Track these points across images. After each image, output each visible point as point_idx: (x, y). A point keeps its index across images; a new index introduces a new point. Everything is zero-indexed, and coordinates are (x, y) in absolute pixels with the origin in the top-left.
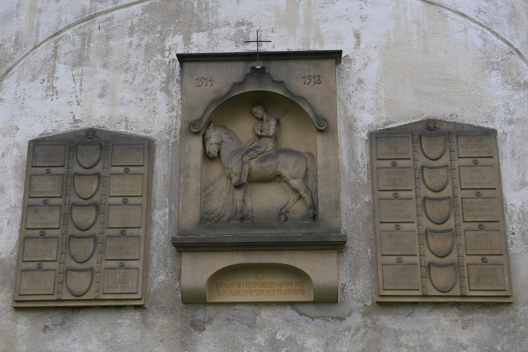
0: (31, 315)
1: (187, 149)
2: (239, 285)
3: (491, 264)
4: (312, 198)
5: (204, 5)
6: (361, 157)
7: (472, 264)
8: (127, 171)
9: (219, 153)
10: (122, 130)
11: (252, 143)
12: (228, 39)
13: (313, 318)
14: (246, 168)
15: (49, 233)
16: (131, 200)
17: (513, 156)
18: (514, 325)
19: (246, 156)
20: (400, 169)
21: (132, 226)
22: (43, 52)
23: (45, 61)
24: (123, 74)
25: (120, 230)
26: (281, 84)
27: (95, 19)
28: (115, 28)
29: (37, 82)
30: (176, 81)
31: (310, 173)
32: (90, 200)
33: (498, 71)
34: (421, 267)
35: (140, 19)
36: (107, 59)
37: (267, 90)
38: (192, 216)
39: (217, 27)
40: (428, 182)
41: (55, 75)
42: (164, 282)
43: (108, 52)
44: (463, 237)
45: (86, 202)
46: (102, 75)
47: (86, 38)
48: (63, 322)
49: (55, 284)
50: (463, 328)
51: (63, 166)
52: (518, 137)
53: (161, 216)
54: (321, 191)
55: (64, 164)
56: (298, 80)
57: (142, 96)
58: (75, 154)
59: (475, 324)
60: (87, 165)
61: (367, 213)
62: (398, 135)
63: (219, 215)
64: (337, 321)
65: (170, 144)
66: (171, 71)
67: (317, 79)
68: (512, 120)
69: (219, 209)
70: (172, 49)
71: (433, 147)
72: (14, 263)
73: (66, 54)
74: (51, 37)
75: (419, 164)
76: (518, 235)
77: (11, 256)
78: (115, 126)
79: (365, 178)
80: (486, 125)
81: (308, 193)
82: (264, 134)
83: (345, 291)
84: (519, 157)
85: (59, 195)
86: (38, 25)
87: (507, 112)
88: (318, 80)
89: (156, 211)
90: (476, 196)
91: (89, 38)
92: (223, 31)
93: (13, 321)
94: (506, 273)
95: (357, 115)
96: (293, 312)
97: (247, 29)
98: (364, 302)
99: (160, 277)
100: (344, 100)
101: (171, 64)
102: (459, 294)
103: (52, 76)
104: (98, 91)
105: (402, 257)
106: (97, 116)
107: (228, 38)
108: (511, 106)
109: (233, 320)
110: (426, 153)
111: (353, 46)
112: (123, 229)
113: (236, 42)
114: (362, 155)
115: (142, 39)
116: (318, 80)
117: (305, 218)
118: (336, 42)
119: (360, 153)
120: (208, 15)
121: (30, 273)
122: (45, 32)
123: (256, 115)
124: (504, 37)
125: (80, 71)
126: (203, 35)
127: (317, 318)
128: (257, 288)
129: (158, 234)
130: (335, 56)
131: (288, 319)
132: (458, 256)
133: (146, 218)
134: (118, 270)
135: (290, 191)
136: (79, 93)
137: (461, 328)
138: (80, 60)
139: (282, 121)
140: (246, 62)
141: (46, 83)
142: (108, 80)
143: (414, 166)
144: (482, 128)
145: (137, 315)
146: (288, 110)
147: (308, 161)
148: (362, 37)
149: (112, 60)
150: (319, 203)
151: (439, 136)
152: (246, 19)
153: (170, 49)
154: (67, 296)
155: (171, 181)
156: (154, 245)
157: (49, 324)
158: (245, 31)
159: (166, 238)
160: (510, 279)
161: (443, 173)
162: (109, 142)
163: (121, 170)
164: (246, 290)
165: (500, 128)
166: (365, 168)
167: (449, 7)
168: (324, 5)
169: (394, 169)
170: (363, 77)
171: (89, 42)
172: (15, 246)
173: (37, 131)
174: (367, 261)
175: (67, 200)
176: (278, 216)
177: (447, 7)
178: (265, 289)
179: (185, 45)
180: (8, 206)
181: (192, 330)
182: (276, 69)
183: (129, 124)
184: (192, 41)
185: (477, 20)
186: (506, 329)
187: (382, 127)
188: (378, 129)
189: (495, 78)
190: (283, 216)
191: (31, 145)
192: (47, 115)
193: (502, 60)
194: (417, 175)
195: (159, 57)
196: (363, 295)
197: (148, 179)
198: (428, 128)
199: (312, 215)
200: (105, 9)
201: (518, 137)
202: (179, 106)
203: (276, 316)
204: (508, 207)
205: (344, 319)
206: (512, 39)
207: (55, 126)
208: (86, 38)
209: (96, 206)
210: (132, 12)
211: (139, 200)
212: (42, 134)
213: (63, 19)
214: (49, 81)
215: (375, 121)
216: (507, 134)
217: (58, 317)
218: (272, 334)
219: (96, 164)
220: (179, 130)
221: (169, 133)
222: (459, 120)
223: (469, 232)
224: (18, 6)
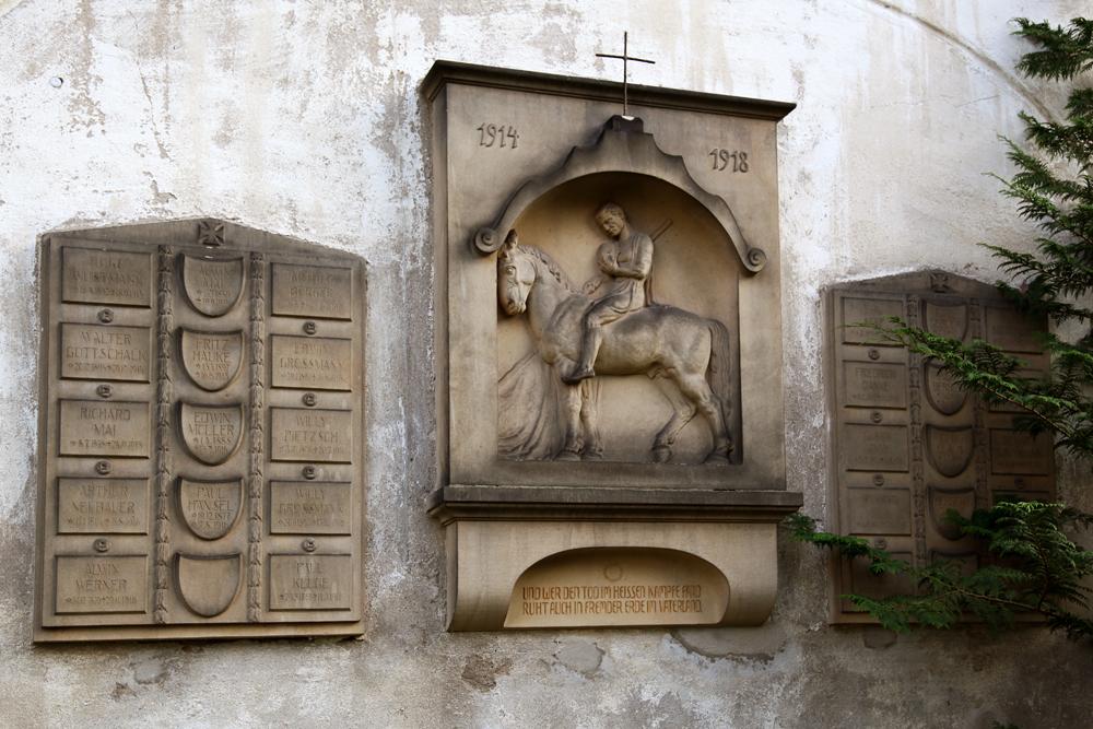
0: (79, 659)
1: (464, 289)
2: (569, 592)
4: (723, 415)
6: (807, 336)
8: (308, 329)
10: (284, 230)
12: (529, 43)
13: (712, 657)
15: (117, 467)
16: (322, 399)
21: (331, 459)
30: (409, 127)
36: (230, 48)
37: (647, 172)
41: (91, 70)
42: (402, 584)
45: (212, 398)
48: (164, 676)
50: (976, 670)
56: (699, 156)
57: (329, 152)
60: (209, 309)
64: (758, 663)
65: (402, 275)
66: (396, 101)
69: (528, 430)
70: (396, 46)
75: (172, 322)
77: (15, 521)
78: (263, 218)
88: (741, 163)
89: (375, 427)
93: (33, 674)
96: (674, 645)
101: (396, 82)
103: (84, 73)
104: (212, 125)
105: (886, 538)
107: (528, 38)
109: (554, 664)
112: (308, 467)
116: (741, 163)
123: (607, 227)
125: (161, 68)
127: (721, 656)
128: (607, 598)
129: (384, 477)
135: (675, 395)
136: (163, 125)
140: (590, 102)
141: (67, 88)
143: (910, 361)
145: (344, 656)
146: (672, 223)
147: (716, 336)
149: (244, 53)
155: (409, 361)
156: (375, 503)
157: (128, 679)
158: (565, 30)
159: (403, 489)
163: (296, 326)
164: (583, 602)
167: (969, 44)
169: (873, 366)
170: (809, 167)
173: (59, 214)
176: (653, 449)
177: (964, 42)
178: (623, 601)
179: (426, 42)
181: (467, 686)
182: (661, 125)
186: (1043, 670)
190: (659, 446)
194: (915, 379)
195: (364, 62)
196: (805, 612)
198: (934, 288)
199: (726, 449)
202: (420, 186)
207: (105, 203)
211: (342, 401)
214: (75, 84)
215: (832, 264)
217: (148, 665)
218: (632, 691)
220: (421, 244)
221: (398, 249)
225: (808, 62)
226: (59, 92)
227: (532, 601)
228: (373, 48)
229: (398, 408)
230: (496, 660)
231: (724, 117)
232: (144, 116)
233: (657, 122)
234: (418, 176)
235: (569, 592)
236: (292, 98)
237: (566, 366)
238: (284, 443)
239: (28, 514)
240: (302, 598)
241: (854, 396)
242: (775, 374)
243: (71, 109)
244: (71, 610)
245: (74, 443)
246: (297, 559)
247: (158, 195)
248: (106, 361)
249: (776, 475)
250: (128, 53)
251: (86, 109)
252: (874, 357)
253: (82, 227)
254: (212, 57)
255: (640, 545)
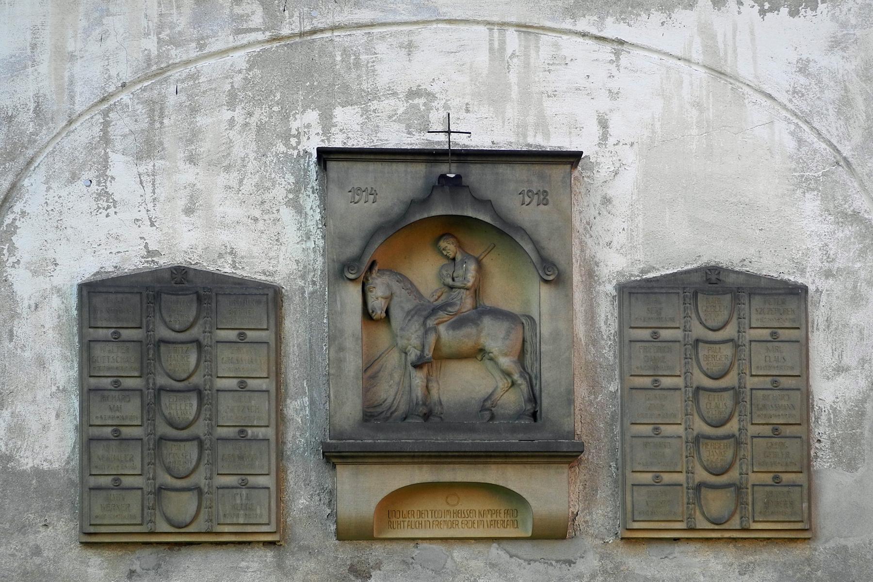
0: (107, 553)
2: (421, 513)
3: (785, 486)
5: (353, 57)
6: (606, 323)
7: (760, 485)
8: (242, 335)
9: (387, 312)
10: (227, 270)
11: (439, 297)
12: (395, 121)
14: (432, 339)
17: (828, 327)
18: (809, 569)
19: (433, 318)
20: (664, 344)
22: (85, 132)
23: (90, 148)
24: (222, 174)
25: (237, 429)
26: (486, 204)
27: (169, 73)
28: (204, 92)
29: (80, 185)
30: (311, 190)
31: (528, 346)
32: (186, 383)
33: (816, 193)
34: (688, 488)
35: (245, 79)
37: (465, 214)
38: (350, 409)
39: (375, 98)
40: (703, 363)
41: (108, 173)
42: (307, 507)
43: (194, 136)
44: (749, 447)
46: (188, 175)
47: (156, 109)
49: (143, 510)
50: (740, 574)
51: (140, 328)
52: (838, 298)
53: (297, 408)
54: (546, 376)
55: (141, 323)
57: (257, 213)
58: (157, 308)
59: (757, 568)
60: (177, 327)
61: (613, 408)
62: (664, 291)
63: (390, 408)
64: (563, 565)
67: (542, 197)
68: (830, 270)
69: (390, 400)
70: (302, 133)
71: (716, 310)
72: (75, 477)
73: (125, 136)
74: (95, 105)
76: (826, 443)
77: (67, 467)
78: (214, 261)
79: (610, 355)
80: (792, 279)
81: (525, 379)
82: (458, 284)
83: (576, 523)
84: (836, 329)
85: (136, 374)
86: (71, 83)
87: (825, 258)
88: (543, 198)
89: (288, 401)
90: (771, 387)
91: (161, 109)
92: (386, 105)
93: (82, 562)
94: (806, 497)
95: (600, 256)
96: (500, 552)
97: (425, 104)
98: (603, 539)
99: (302, 500)
100: (581, 230)
102: (738, 527)
103: (104, 174)
104: (182, 203)
105: (662, 474)
106: (185, 246)
108: (831, 249)
109: (412, 563)
110: (703, 320)
111: (597, 141)
113: (408, 127)
114: (607, 319)
115: (250, 114)
117: (519, 415)
118: (570, 133)
119: (603, 316)
120: (359, 76)
121: (103, 493)
122: (83, 98)
123: (445, 253)
124: (828, 137)
125: (150, 167)
126: (353, 111)
127: (535, 561)
128: (448, 518)
130: (573, 158)
131: (494, 562)
132: (741, 474)
133: (277, 412)
134: (238, 491)
135: (498, 375)
137: (737, 573)
138: (148, 148)
139: (487, 261)
140: (429, 164)
141: (94, 187)
142: (198, 184)
143: (685, 339)
144: (786, 283)
145: (269, 555)
148: (611, 126)
150: (543, 394)
151: (724, 293)
152: (423, 87)
153: (299, 133)
154: (165, 527)
157: (137, 566)
159: (307, 443)
160: (810, 507)
161: (727, 351)
162: (210, 290)
164: (431, 521)
165: (813, 283)
166: (610, 339)
167: (748, 82)
168: (551, 67)
170: (610, 193)
171: (162, 116)
172: (73, 451)
173: (88, 268)
174: (610, 479)
175: (151, 381)
178: (460, 520)
180: (54, 389)
183: (237, 260)
184: (334, 120)
185: (790, 106)
187: (638, 276)
188: (633, 278)
189: (811, 204)
190: (487, 408)
191: (85, 293)
192: (103, 242)
193: (823, 175)
195: (282, 148)
197: (276, 351)
198: (709, 281)
199: (532, 411)
200: (185, 58)
201: (838, 298)
202: (318, 232)
203: (476, 558)
204: (815, 403)
205: (575, 563)
206: (839, 142)
207: (116, 260)
208: (156, 109)
209: (199, 392)
210: (232, 66)
212: (98, 273)
213: (113, 73)
215: (627, 266)
216: (821, 292)
219: (191, 326)
221: (303, 277)
222: (752, 269)
223: (758, 439)
224: (34, 47)
225: (611, 111)
226: (89, 189)
227: (394, 519)
228: (286, 137)
229: (304, 388)
230: (372, 561)
231: (523, 166)
232: (140, 200)
233: (475, 174)
234: (317, 225)
235: (421, 513)
236: (233, 178)
237: (413, 355)
238: (225, 414)
239: (75, 463)
240: (238, 516)
241: (637, 368)
242: (567, 354)
243: (96, 200)
244: (98, 523)
245: (97, 417)
246: (234, 491)
247: (148, 252)
248: (116, 365)
249: (567, 429)
250: (130, 159)
251: (105, 199)
252: (655, 336)
253: (104, 277)
254: (182, 155)
255: (465, 480)
